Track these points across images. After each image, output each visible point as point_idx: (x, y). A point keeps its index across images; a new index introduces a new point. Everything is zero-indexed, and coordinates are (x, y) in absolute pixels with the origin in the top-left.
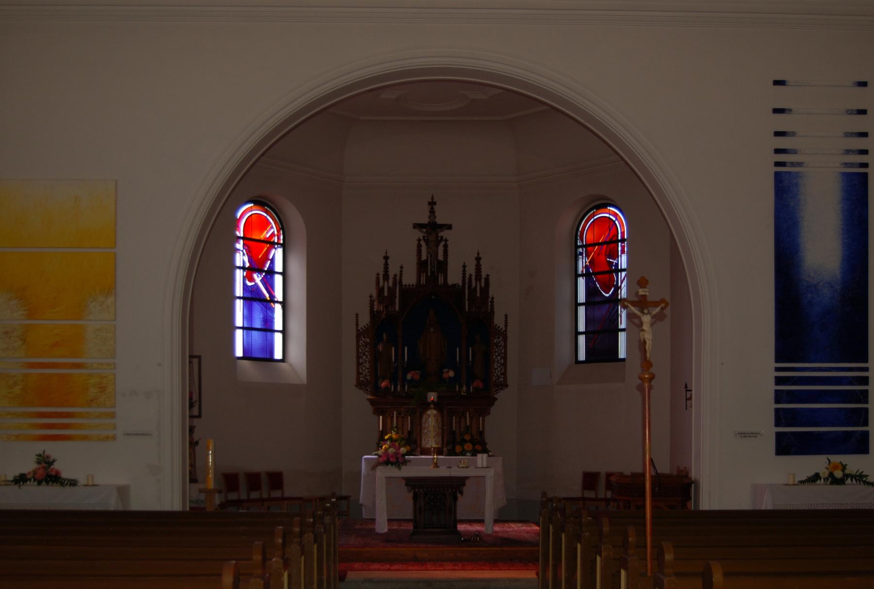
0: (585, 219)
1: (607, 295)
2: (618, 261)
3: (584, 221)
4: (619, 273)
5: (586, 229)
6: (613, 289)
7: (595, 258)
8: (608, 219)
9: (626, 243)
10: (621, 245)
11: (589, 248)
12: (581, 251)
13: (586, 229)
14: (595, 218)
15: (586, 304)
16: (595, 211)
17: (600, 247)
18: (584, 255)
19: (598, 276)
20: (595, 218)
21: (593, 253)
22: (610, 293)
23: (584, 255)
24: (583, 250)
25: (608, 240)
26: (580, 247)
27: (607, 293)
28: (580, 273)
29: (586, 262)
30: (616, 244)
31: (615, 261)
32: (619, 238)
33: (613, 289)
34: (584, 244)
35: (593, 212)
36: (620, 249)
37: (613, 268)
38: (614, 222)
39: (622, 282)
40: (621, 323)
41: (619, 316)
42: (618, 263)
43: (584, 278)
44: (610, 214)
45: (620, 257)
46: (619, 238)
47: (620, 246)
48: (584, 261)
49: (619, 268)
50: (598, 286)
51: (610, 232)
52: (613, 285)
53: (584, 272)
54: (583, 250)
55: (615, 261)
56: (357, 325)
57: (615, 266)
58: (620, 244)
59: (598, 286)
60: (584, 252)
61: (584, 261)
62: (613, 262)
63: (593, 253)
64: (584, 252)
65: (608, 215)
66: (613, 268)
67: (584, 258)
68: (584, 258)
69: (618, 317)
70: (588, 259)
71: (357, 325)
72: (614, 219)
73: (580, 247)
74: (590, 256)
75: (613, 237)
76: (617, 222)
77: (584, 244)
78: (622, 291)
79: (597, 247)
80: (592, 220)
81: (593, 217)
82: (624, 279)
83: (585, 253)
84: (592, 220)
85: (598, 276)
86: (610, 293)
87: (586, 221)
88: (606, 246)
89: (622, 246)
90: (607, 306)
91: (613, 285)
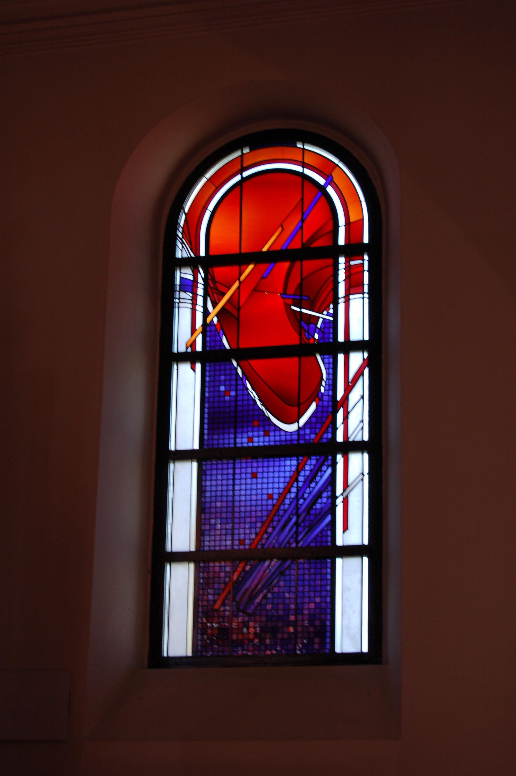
0: (209, 175)
1: (292, 428)
2: (335, 315)
3: (203, 181)
4: (341, 357)
5: (211, 207)
6: (313, 407)
7: (242, 302)
8: (300, 179)
9: (366, 257)
10: (347, 262)
11: (219, 271)
12: (191, 278)
13: (211, 207)
14: (246, 174)
15: (301, 312)
16: (246, 150)
17: (264, 266)
18: (200, 291)
19: (256, 364)
20: (246, 174)
21: (236, 285)
22: (303, 420)
23: (200, 291)
24: (195, 275)
25: (297, 245)
26: (184, 263)
27: (289, 422)
28: (182, 349)
29: (206, 313)
30: (330, 261)
31: (323, 316)
32: (341, 241)
33: (313, 407)
34: (202, 253)
35: (238, 154)
36: (342, 276)
37: (316, 336)
38: (322, 189)
39: (349, 388)
40: (346, 528)
41: (339, 501)
42: (335, 322)
43: (198, 366)
44: (304, 165)
45: (341, 302)
46: (341, 241)
47: (342, 266)
48: (200, 309)
49: (341, 338)
50: (253, 394)
51: (302, 221)
52: (316, 396)
53: (199, 348)
54: (195, 275)
55: (323, 316)
56: (219, 283)
57: (321, 331)
58: (342, 260)
59: (253, 394)
60: (200, 280)
61: (200, 309)
62: (318, 318)
63: (236, 285)
64: (200, 280)
65: (298, 169)
66: (316, 336)
67: (200, 301)
68: (200, 301)
69: (334, 506)
70: (214, 306)
71: (219, 283)
72: (321, 181)
73: (184, 263)
74: (223, 295)
75: (313, 238)
76: (330, 189)
77: (202, 253)
78: (351, 417)
79: (251, 267)
80: (238, 178)
81: (241, 172)
82: (359, 373)
83: (206, 285)
84: (238, 178)
85: (254, 363)
86: (303, 420)
87: (209, 180)
88: (286, 265)
89: (348, 268)
90: (291, 464)
91: (316, 396)
